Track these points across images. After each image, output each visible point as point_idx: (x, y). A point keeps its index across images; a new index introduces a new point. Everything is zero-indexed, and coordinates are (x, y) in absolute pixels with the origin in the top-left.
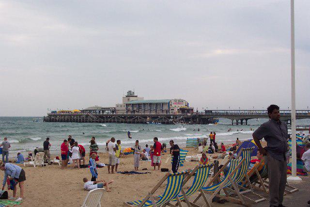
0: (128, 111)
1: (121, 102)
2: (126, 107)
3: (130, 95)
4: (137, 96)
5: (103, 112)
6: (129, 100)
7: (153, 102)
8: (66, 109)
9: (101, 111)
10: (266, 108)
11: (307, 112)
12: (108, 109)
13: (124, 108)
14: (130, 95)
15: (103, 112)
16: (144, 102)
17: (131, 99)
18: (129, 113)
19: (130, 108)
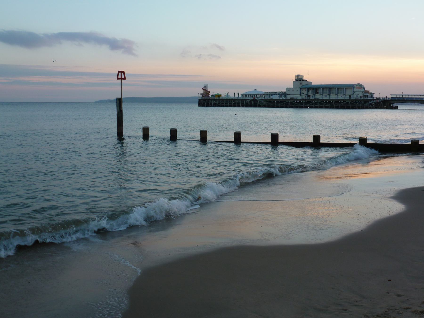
0: (301, 94)
1: (291, 86)
2: (299, 90)
4: (306, 80)
12: (275, 93)
17: (304, 83)
19: (305, 92)
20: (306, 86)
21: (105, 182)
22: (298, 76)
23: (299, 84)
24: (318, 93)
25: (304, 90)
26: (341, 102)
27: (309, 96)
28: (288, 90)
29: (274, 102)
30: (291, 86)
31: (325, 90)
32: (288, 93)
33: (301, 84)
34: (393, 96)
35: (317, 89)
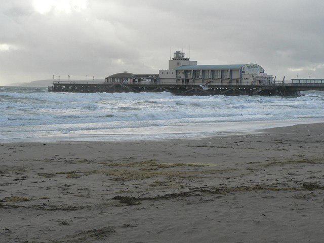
0: (178, 79)
1: (166, 67)
2: (175, 73)
3: (179, 57)
4: (187, 60)
5: (139, 81)
6: (178, 64)
7: (226, 68)
8: (157, 94)
9: (137, 80)
10: (104, 79)
11: (320, 82)
12: (146, 76)
13: (174, 76)
14: (179, 57)
15: (139, 81)
16: (213, 68)
17: (182, 62)
18: (180, 83)
19: (182, 76)
20: (183, 68)
21: (315, 175)
22: (178, 53)
23: (176, 63)
24: (198, 77)
25: (181, 73)
26: (186, 89)
27: (188, 81)
28: (162, 72)
29: (145, 89)
30: (166, 67)
31: (233, 72)
32: (161, 76)
33: (178, 64)
34: (294, 82)
35: (197, 72)
